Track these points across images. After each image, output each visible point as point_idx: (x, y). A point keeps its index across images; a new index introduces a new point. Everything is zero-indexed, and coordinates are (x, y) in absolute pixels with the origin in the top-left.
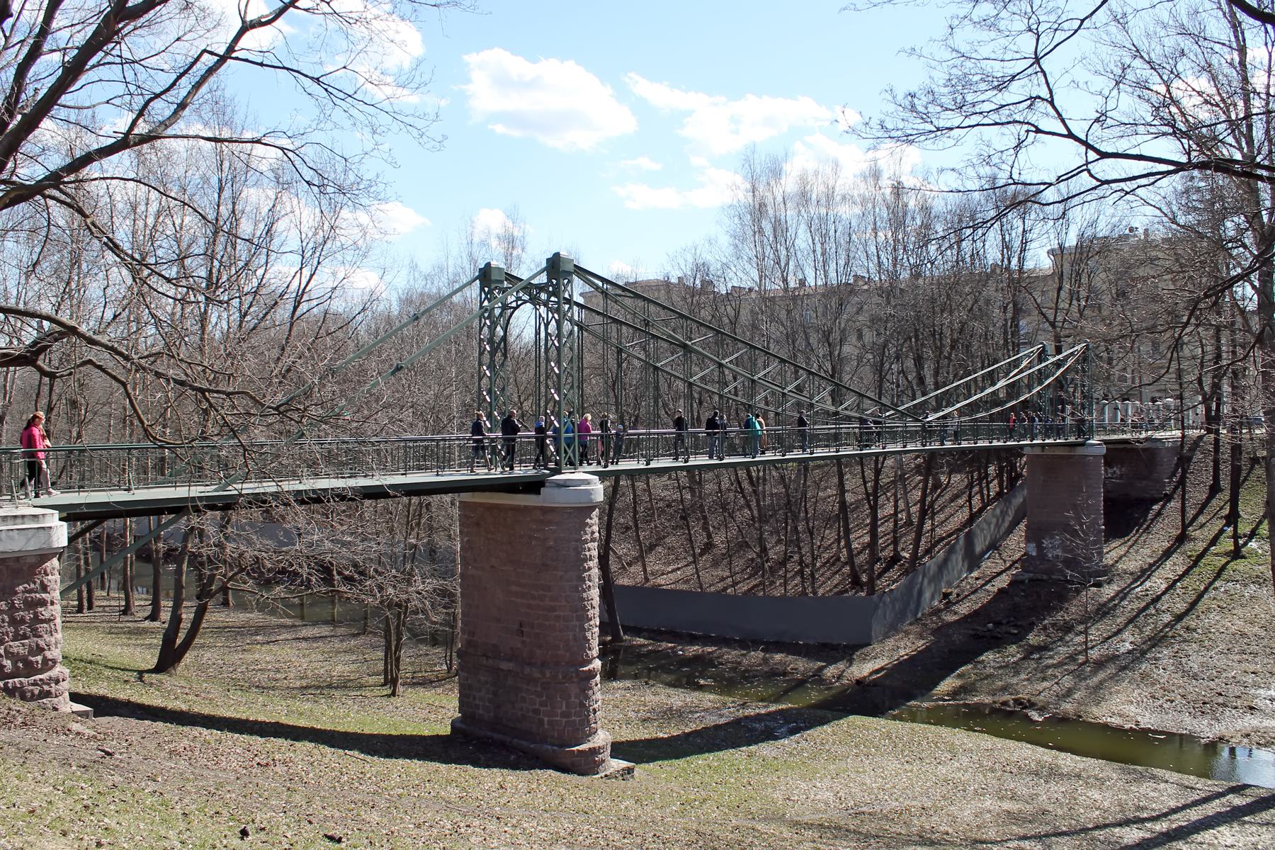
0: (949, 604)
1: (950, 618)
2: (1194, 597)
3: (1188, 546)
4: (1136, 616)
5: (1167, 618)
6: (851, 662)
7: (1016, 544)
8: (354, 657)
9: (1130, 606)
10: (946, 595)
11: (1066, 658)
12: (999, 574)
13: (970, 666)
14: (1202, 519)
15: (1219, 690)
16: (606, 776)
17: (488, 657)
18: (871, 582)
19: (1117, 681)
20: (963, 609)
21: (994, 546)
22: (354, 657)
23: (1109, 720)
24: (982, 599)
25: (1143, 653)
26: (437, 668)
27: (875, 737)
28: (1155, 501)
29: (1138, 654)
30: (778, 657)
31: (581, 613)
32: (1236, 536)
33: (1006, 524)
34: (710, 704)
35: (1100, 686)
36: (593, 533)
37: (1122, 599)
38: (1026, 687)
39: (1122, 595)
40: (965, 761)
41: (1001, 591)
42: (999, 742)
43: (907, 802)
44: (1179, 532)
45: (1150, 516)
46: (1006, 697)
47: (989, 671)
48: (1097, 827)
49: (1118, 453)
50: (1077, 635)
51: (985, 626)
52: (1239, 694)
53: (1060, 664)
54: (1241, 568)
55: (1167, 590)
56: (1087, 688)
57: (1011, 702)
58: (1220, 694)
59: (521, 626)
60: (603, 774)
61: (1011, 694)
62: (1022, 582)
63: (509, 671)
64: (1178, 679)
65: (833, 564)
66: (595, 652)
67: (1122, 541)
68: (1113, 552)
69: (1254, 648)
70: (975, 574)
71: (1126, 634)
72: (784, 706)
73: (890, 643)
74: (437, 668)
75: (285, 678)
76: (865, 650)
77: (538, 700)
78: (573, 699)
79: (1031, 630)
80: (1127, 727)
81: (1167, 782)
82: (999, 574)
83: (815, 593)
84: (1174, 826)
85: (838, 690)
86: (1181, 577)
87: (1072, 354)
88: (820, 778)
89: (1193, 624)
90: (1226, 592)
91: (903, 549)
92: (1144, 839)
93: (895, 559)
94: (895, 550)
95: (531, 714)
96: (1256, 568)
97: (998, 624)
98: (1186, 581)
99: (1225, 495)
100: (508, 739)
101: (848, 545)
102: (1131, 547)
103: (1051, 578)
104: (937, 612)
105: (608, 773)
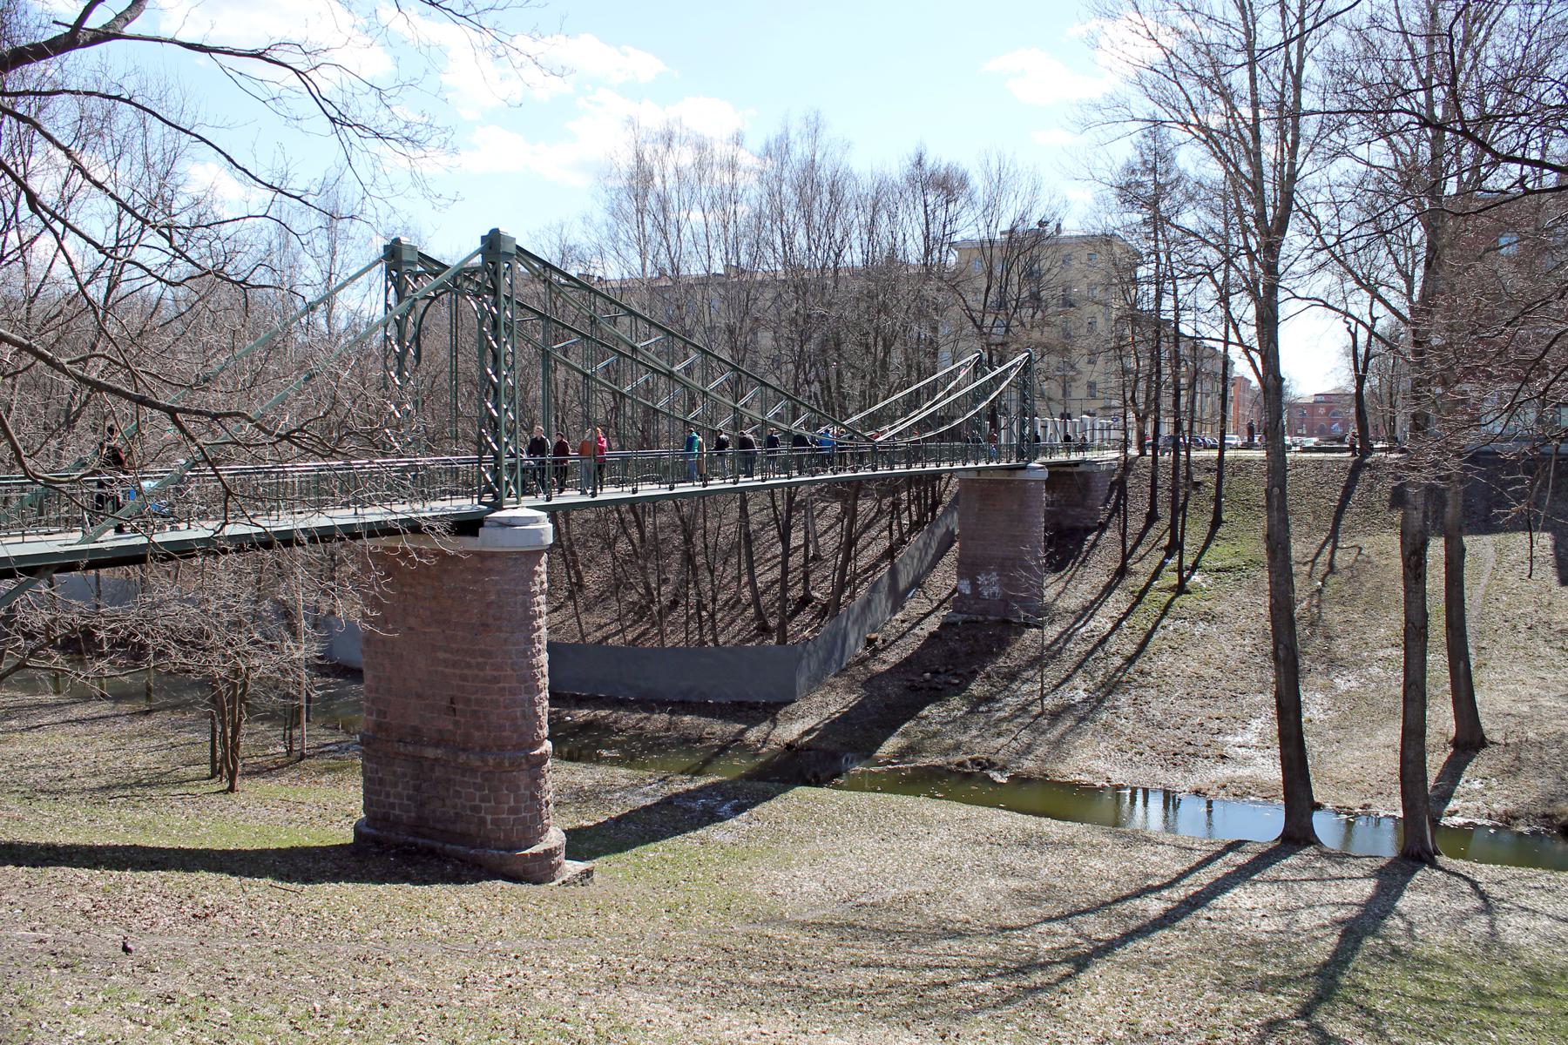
0: (876, 651)
1: (879, 668)
2: (1142, 637)
3: (1129, 581)
4: (1085, 660)
5: (1118, 661)
6: (775, 723)
7: (944, 579)
8: (155, 742)
9: (1076, 649)
10: (870, 642)
11: (1019, 710)
12: (927, 615)
13: (913, 723)
14: (1141, 551)
15: (1187, 739)
16: (564, 882)
17: (406, 744)
18: (782, 627)
19: (1080, 734)
20: (893, 657)
21: (917, 583)
22: (155, 742)
23: (1077, 778)
24: (911, 645)
25: (1100, 701)
26: (270, 751)
27: (834, 812)
28: (1089, 531)
29: (1095, 703)
30: (687, 719)
31: (530, 683)
32: (1180, 570)
33: (929, 558)
34: (626, 781)
35: (1057, 743)
36: (542, 583)
37: (1067, 641)
38: (978, 743)
39: (1066, 636)
40: (944, 833)
41: (932, 635)
42: (975, 811)
43: (906, 889)
44: (1118, 565)
45: (1085, 548)
46: (960, 757)
47: (934, 727)
48: (1116, 901)
49: (1060, 475)
50: (1024, 683)
51: (921, 675)
52: (1208, 742)
53: (1013, 717)
54: (1188, 604)
55: (1113, 630)
56: (1050, 743)
57: (969, 763)
58: (1189, 744)
59: (452, 702)
60: (560, 881)
61: (966, 753)
62: (955, 624)
63: (436, 759)
64: (1142, 730)
65: (733, 607)
66: (545, 732)
67: (1058, 575)
68: (1052, 587)
69: (1212, 691)
70: (899, 616)
71: (1077, 681)
72: (711, 780)
73: (817, 698)
74: (270, 751)
75: (72, 776)
76: (793, 707)
77: (478, 794)
78: (523, 791)
79: (973, 679)
80: (1098, 784)
81: (1163, 844)
82: (927, 615)
83: (715, 640)
84: (1191, 892)
85: (767, 757)
86: (1126, 615)
87: (1014, 366)
88: (797, 865)
89: (1146, 668)
90: (1175, 630)
91: (813, 588)
92: (1167, 910)
93: (805, 601)
94: (805, 588)
95: (469, 812)
96: (1203, 603)
97: (936, 673)
98: (1132, 620)
99: (1165, 521)
100: (439, 845)
101: (752, 582)
102: (1068, 582)
103: (986, 620)
104: (862, 661)
105: (566, 878)
